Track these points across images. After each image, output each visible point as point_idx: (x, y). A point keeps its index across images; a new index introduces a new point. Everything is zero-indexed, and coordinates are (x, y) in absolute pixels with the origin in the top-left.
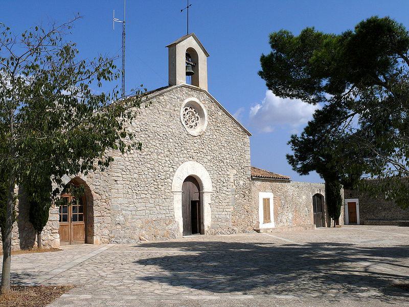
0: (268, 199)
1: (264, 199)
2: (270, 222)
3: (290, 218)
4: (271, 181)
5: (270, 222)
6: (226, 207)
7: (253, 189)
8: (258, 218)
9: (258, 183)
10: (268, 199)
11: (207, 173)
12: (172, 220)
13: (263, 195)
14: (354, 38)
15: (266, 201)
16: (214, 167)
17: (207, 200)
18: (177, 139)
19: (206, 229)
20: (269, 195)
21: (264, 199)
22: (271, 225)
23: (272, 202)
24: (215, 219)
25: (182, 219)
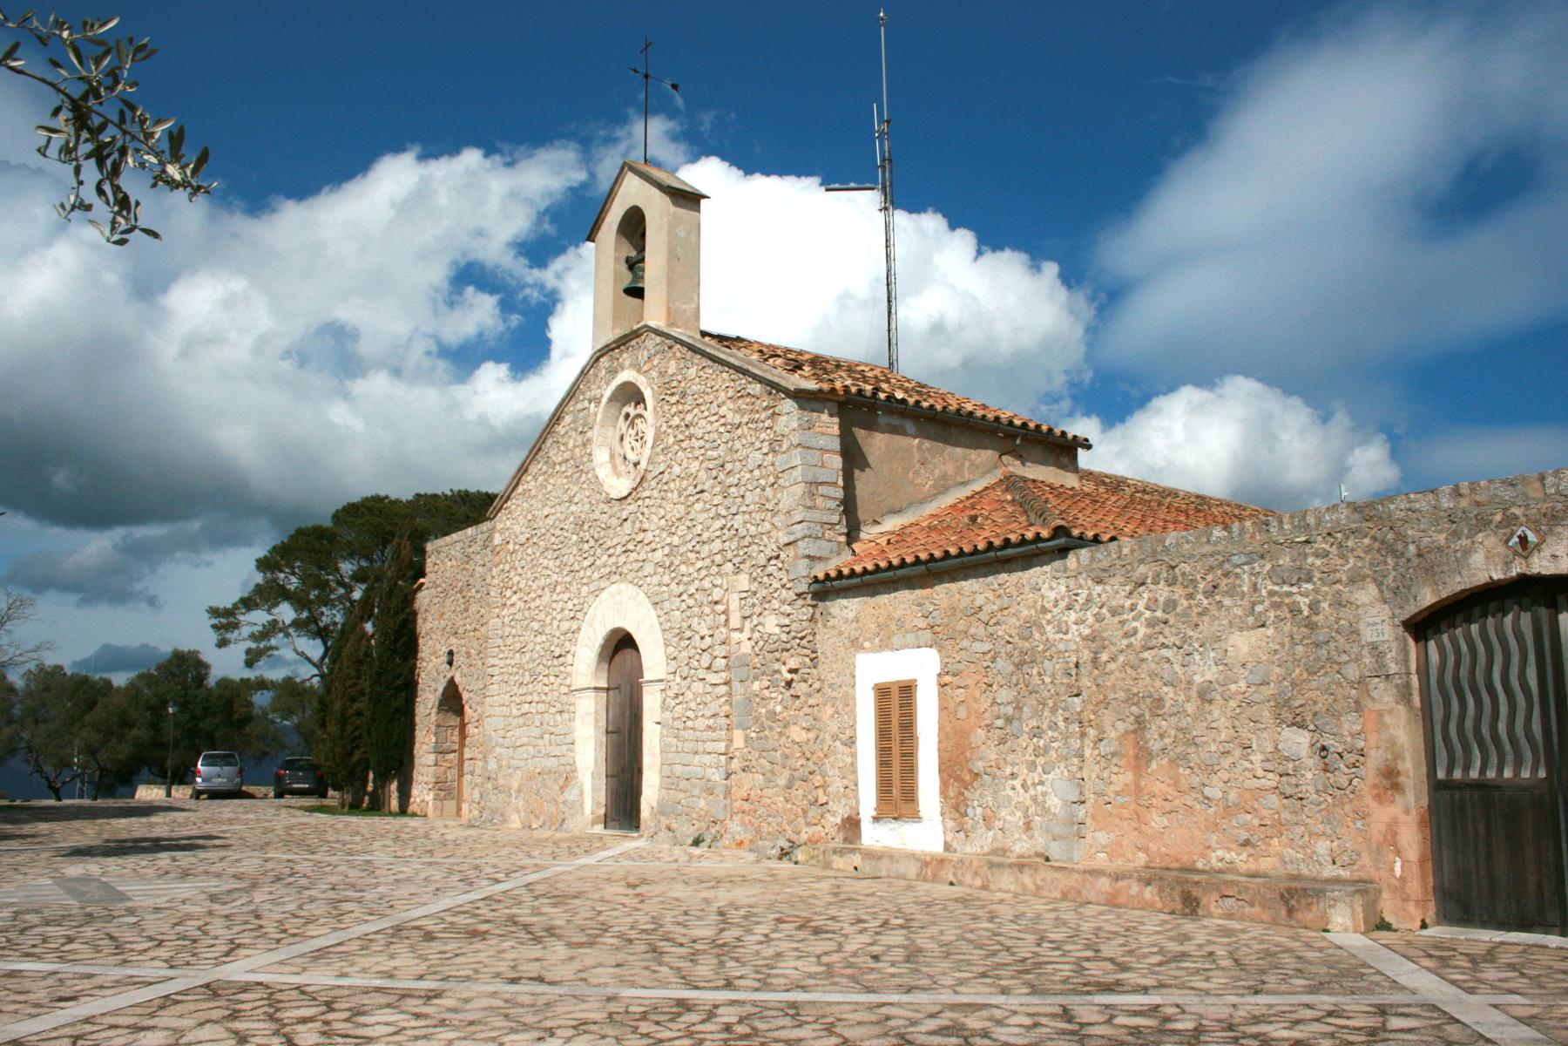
0: (907, 690)
1: (882, 692)
2: (915, 816)
3: (1054, 803)
4: (910, 583)
5: (915, 816)
6: (705, 735)
7: (826, 641)
8: (852, 789)
9: (846, 609)
10: (907, 690)
11: (653, 613)
12: (568, 777)
13: (875, 668)
14: (327, 183)
15: (896, 702)
16: (673, 585)
17: (651, 703)
18: (558, 532)
19: (645, 813)
20: (919, 666)
21: (882, 692)
22: (925, 834)
23: (653, 659)
24: (670, 781)
25: (418, 719)
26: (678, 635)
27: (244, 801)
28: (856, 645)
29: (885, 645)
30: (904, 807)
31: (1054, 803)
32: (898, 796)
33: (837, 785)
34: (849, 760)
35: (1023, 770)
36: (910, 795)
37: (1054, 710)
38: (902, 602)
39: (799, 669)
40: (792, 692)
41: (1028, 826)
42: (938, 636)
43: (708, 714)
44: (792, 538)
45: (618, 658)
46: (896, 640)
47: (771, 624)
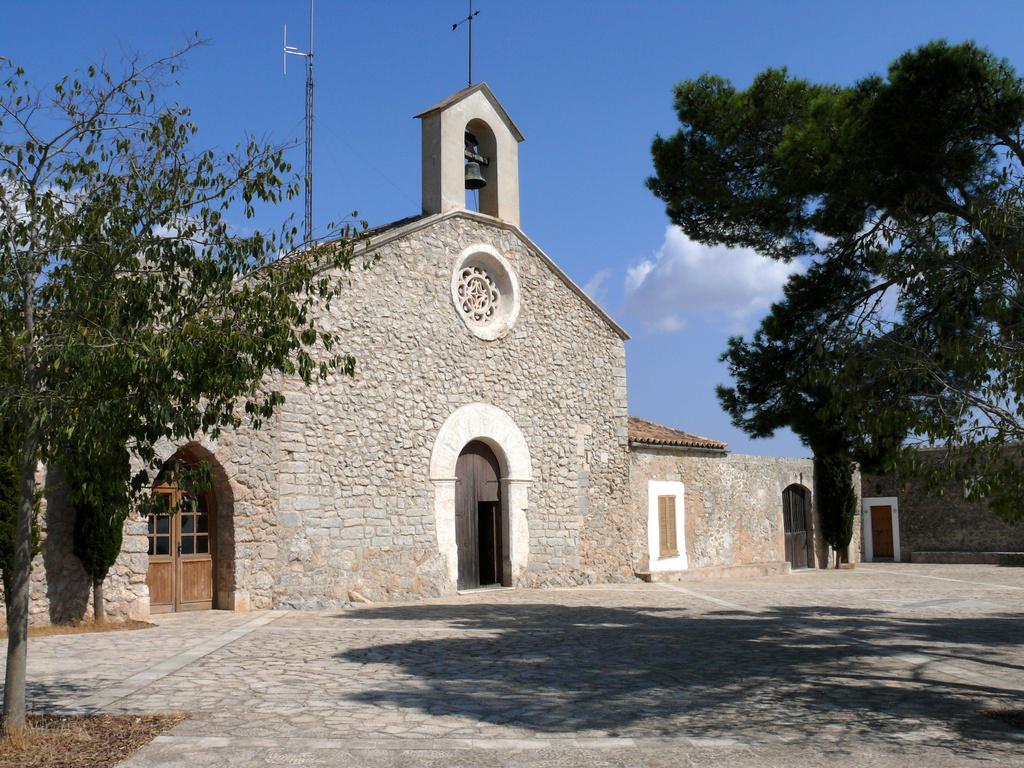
0: (672, 499)
4: (678, 453)
7: (634, 472)
8: (645, 544)
9: (646, 458)
10: (672, 499)
12: (430, 550)
13: (657, 489)
15: (667, 504)
19: (516, 572)
20: (675, 488)
22: (680, 563)
23: (520, 463)
24: (539, 548)
26: (541, 455)
27: (150, 629)
28: (649, 476)
29: (663, 478)
30: (672, 552)
31: (726, 545)
32: (668, 547)
33: (638, 542)
34: (643, 531)
35: (716, 534)
36: (674, 546)
37: (725, 511)
38: (670, 460)
39: (616, 485)
40: (613, 496)
41: (718, 553)
42: (684, 478)
43: (566, 505)
44: (620, 414)
45: (470, 457)
46: (667, 476)
47: (604, 457)
